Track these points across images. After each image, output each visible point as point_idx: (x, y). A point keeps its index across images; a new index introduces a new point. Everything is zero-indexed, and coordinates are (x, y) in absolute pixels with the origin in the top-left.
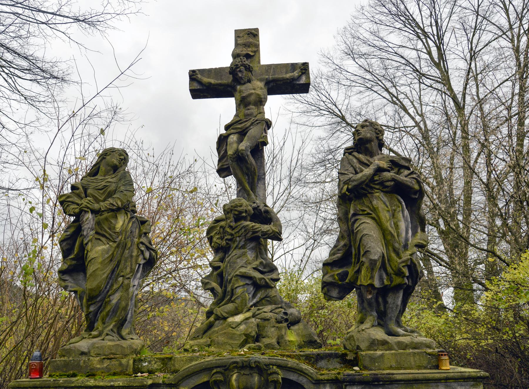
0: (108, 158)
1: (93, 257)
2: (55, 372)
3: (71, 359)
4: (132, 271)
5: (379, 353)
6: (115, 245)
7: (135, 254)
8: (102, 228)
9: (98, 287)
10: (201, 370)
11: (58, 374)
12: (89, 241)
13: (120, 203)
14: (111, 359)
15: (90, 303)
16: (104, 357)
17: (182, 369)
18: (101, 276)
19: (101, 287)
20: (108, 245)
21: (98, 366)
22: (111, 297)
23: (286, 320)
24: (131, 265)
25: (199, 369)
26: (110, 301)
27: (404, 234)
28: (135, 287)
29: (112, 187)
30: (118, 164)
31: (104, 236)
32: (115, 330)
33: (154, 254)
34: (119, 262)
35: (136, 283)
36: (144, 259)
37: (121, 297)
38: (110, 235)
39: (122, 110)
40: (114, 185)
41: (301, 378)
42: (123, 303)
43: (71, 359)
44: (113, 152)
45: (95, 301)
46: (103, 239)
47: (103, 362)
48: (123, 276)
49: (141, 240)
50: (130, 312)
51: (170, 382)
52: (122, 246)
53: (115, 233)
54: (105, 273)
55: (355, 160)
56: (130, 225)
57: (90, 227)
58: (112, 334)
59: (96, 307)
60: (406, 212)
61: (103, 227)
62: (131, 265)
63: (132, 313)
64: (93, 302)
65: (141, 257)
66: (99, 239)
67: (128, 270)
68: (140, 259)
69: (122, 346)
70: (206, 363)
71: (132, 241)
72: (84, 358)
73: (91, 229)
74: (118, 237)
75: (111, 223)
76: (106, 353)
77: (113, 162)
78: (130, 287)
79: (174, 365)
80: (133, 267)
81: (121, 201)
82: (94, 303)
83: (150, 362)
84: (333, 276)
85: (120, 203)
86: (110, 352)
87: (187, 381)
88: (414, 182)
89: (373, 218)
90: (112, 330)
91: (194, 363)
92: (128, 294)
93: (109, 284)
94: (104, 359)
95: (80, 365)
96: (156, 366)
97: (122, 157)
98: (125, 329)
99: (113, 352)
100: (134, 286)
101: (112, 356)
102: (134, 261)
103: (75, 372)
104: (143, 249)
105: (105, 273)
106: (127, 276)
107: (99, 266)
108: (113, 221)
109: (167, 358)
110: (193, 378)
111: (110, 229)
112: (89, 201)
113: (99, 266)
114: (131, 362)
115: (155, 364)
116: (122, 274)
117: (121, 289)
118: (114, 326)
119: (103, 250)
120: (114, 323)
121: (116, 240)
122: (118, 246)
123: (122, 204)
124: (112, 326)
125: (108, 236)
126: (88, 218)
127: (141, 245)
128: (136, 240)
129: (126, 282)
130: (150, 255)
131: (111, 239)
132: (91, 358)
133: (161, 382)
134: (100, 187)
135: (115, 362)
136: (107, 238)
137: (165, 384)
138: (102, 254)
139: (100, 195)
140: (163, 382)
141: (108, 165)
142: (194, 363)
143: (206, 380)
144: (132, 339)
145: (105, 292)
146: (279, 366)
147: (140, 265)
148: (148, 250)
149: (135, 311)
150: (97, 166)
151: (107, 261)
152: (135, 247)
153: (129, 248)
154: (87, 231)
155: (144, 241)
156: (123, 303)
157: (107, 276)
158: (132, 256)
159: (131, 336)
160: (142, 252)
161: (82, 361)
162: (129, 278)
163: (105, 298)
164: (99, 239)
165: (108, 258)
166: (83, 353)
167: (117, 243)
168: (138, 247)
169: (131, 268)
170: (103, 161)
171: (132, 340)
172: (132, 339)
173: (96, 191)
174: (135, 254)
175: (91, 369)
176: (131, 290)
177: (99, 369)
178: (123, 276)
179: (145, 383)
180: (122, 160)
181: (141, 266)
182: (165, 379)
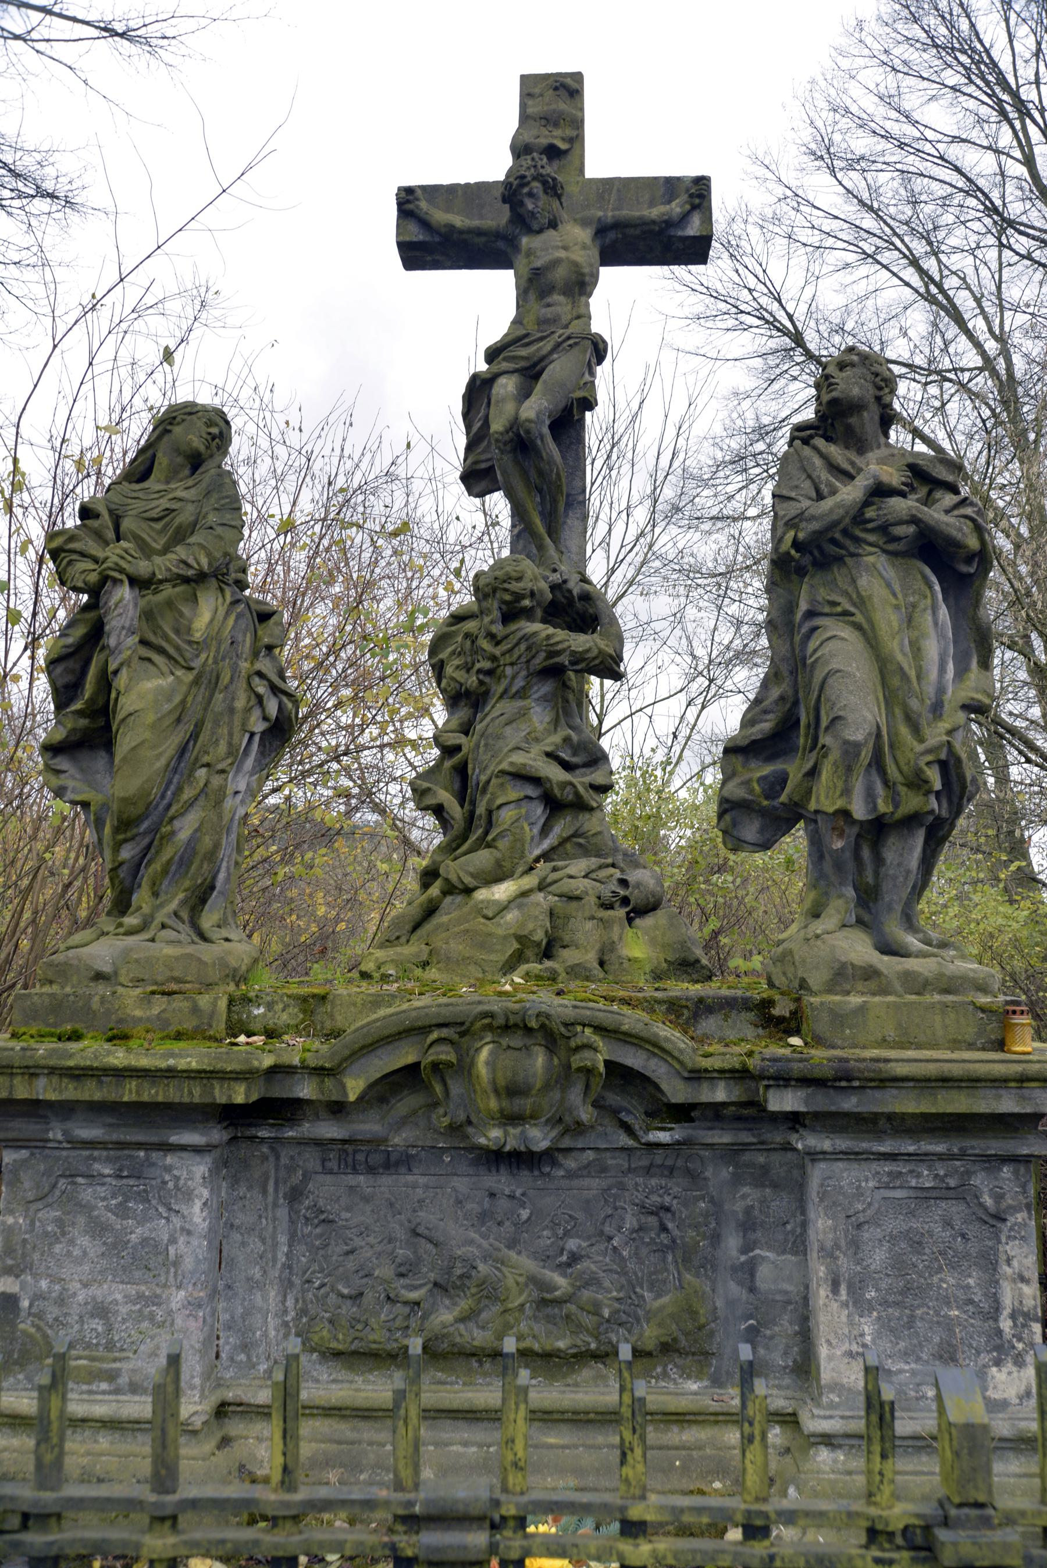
0: (177, 430)
1: (131, 709)
2: (26, 1024)
3: (68, 990)
4: (232, 751)
6: (190, 677)
7: (240, 704)
8: (156, 629)
11: (33, 1031)
12: (122, 664)
13: (204, 562)
15: (121, 837)
21: (138, 1013)
22: (177, 824)
23: (625, 901)
24: (231, 734)
25: (394, 1030)
26: (173, 833)
27: (933, 675)
31: (161, 651)
33: (290, 705)
34: (199, 726)
35: (242, 786)
36: (265, 718)
38: (178, 648)
41: (653, 1063)
45: (135, 831)
48: (207, 765)
49: (258, 666)
52: (208, 682)
54: (160, 754)
55: (818, 462)
56: (231, 621)
59: (138, 850)
60: (943, 612)
62: (231, 734)
64: (129, 834)
65: (257, 713)
67: (222, 748)
68: (253, 719)
69: (199, 960)
70: (414, 1014)
71: (235, 668)
72: (102, 989)
79: (332, 1016)
80: (236, 740)
81: (209, 555)
82: (132, 839)
83: (270, 1006)
86: (168, 974)
88: (967, 527)
89: (858, 627)
91: (382, 1012)
92: (220, 817)
93: (172, 787)
94: (153, 993)
96: (285, 1016)
99: (176, 974)
101: (174, 987)
103: (78, 1026)
104: (261, 690)
105: (160, 754)
106: (220, 767)
107: (147, 735)
108: (186, 610)
109: (314, 996)
110: (379, 1052)
111: (177, 632)
113: (147, 735)
114: (223, 1004)
116: (206, 759)
117: (201, 801)
118: (183, 903)
120: (181, 896)
122: (196, 682)
124: (176, 902)
125: (171, 651)
127: (256, 680)
128: (244, 665)
129: (216, 781)
130: (281, 708)
132: (120, 990)
133: (296, 1061)
134: (154, 514)
135: (179, 1003)
136: (170, 657)
140: (302, 1061)
141: (178, 451)
142: (382, 1012)
143: (411, 1059)
144: (227, 940)
147: (252, 734)
150: (149, 453)
151: (167, 722)
155: (264, 670)
156: (207, 842)
158: (232, 710)
159: (224, 933)
160: (260, 698)
161: (97, 999)
162: (223, 771)
164: (149, 660)
165: (170, 712)
166: (99, 976)
169: (230, 744)
170: (166, 439)
172: (227, 940)
173: (144, 525)
174: (240, 704)
175: (120, 1021)
176: (229, 803)
177: (140, 1019)
178: (207, 765)
179: (256, 1063)
181: (257, 738)
182: (307, 1055)
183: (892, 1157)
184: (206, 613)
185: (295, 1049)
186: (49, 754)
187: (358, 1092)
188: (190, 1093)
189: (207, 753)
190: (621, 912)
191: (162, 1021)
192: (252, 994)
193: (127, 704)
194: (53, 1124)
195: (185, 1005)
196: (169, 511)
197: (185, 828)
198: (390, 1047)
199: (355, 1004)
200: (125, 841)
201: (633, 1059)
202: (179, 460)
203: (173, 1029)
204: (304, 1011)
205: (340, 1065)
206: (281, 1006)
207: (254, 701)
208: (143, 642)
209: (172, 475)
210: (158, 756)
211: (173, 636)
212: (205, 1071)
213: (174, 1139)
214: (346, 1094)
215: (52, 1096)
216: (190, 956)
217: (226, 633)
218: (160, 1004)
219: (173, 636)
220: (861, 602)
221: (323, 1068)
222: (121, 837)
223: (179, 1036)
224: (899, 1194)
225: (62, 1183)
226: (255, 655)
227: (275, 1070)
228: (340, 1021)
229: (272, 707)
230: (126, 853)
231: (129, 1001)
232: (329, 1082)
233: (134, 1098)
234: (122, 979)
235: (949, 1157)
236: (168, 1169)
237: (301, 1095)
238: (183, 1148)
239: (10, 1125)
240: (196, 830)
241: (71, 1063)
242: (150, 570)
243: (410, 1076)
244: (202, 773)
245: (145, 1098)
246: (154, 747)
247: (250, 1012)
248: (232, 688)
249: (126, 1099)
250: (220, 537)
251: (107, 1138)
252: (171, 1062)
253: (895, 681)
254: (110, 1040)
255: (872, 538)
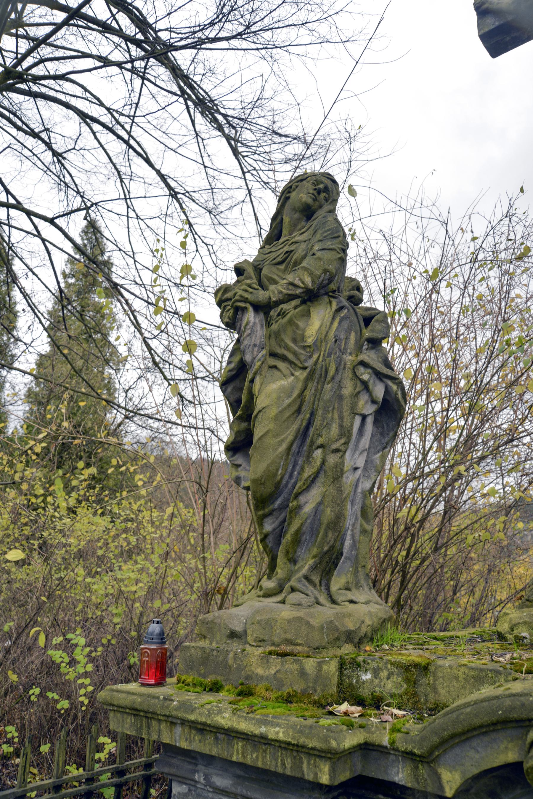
0: (293, 195)
1: (264, 405)
2: (187, 673)
3: (214, 645)
4: (345, 433)
6: (305, 374)
7: (348, 390)
8: (281, 343)
9: (270, 474)
10: (494, 724)
11: (189, 680)
12: (255, 374)
13: (308, 280)
14: (284, 655)
15: (260, 513)
16: (273, 648)
17: (456, 704)
18: (275, 450)
19: (275, 475)
20: (293, 378)
21: (260, 671)
22: (302, 499)
24: (341, 418)
25: (486, 720)
26: (299, 507)
28: (359, 472)
29: (300, 251)
30: (310, 201)
31: (284, 359)
32: (316, 579)
33: (395, 387)
34: (313, 414)
35: (361, 462)
36: (374, 402)
37: (323, 497)
38: (295, 354)
39: (363, 132)
40: (303, 246)
42: (328, 511)
43: (214, 645)
44: (302, 180)
45: (271, 507)
46: (281, 365)
47: (268, 662)
48: (322, 446)
49: (361, 357)
50: (349, 532)
51: (410, 748)
52: (316, 376)
53: (304, 348)
54: (283, 441)
56: (336, 324)
57: (258, 343)
58: (304, 589)
59: (277, 523)
61: (282, 340)
62: (341, 418)
63: (353, 536)
64: (267, 510)
65: (364, 398)
66: (275, 367)
67: (335, 430)
68: (361, 403)
69: (308, 623)
70: (508, 702)
71: (339, 363)
72: (235, 646)
73: (259, 346)
74: (310, 357)
75: (297, 327)
76: (276, 640)
77: (300, 201)
78: (342, 473)
79: (435, 689)
80: (346, 422)
81: (311, 274)
82: (270, 514)
83: (376, 672)
85: (308, 280)
86: (283, 636)
87: (457, 750)
90: (306, 578)
91: (487, 691)
92: (340, 491)
93: (298, 468)
94: (270, 653)
95: (227, 663)
96: (390, 685)
97: (321, 186)
98: (339, 575)
99: (289, 636)
100: (356, 469)
101: (288, 649)
102: (346, 408)
103: (220, 678)
104: (365, 377)
105: (283, 441)
106: (334, 447)
107: (271, 426)
108: (301, 324)
109: (416, 665)
110: (475, 743)
111: (295, 341)
112: (250, 286)
113: (271, 426)
114: (332, 667)
115: (388, 678)
116: (320, 441)
117: (322, 478)
118: (314, 568)
119: (282, 389)
120: (311, 562)
121: (306, 364)
122: (310, 378)
123: (313, 282)
124: (307, 567)
125: (290, 356)
126: (247, 324)
127: (361, 369)
128: (349, 359)
129: (332, 459)
130: (387, 390)
131: (297, 362)
132: (248, 648)
133: (385, 741)
134: (279, 259)
135: (290, 665)
136: (291, 363)
137: (397, 750)
138: (279, 398)
139: (280, 274)
140: (393, 743)
141: (294, 210)
142: (487, 691)
143: (511, 757)
144: (352, 602)
145: (290, 486)
147: (364, 417)
148: (381, 380)
149: (364, 532)
150: (279, 218)
151: (287, 414)
152: (348, 374)
153: (333, 378)
154: (252, 352)
155: (366, 359)
156: (328, 513)
157: (289, 448)
158: (340, 398)
159: (350, 595)
160: (365, 385)
161: (231, 655)
162: (337, 451)
163: (288, 500)
164: (275, 367)
165: (289, 405)
166: (233, 635)
167: (308, 370)
168: (354, 373)
169: (341, 426)
170: (287, 204)
171: (352, 606)
172: (352, 602)
173: (274, 269)
174: (348, 390)
175: (248, 677)
176: (349, 479)
177: (262, 677)
178: (322, 446)
179: (334, 744)
180: (319, 193)
181: (370, 420)
182: (398, 735)
184: (318, 321)
185: (393, 725)
186: (230, 453)
187: (455, 786)
188: (283, 764)
189: (320, 435)
191: (277, 681)
192: (360, 659)
193: (260, 403)
194: (200, 767)
195: (295, 667)
196: (289, 253)
197: (310, 502)
198: (486, 739)
199: (457, 678)
200: (265, 516)
202: (297, 215)
203: (286, 690)
204: (407, 681)
205: (431, 752)
206: (385, 674)
207: (359, 387)
208: (273, 355)
209: (294, 226)
210: (280, 443)
211: (292, 345)
212: (289, 744)
214: (441, 787)
215: (184, 745)
216: (300, 619)
217: (332, 335)
218: (276, 663)
219: (292, 345)
221: (412, 753)
222: (260, 513)
223: (288, 700)
226: (359, 349)
227: (367, 748)
228: (443, 694)
229: (379, 391)
230: (269, 526)
231: (254, 660)
232: (423, 770)
233: (241, 760)
234: (250, 639)
237: (396, 779)
239: (174, 761)
240: (320, 504)
241: (192, 717)
242: (267, 296)
244: (318, 454)
245: (249, 761)
246: (277, 435)
247: (358, 677)
248: (338, 378)
249: (234, 759)
250: (320, 259)
251: (233, 790)
252: (263, 729)
254: (239, 694)
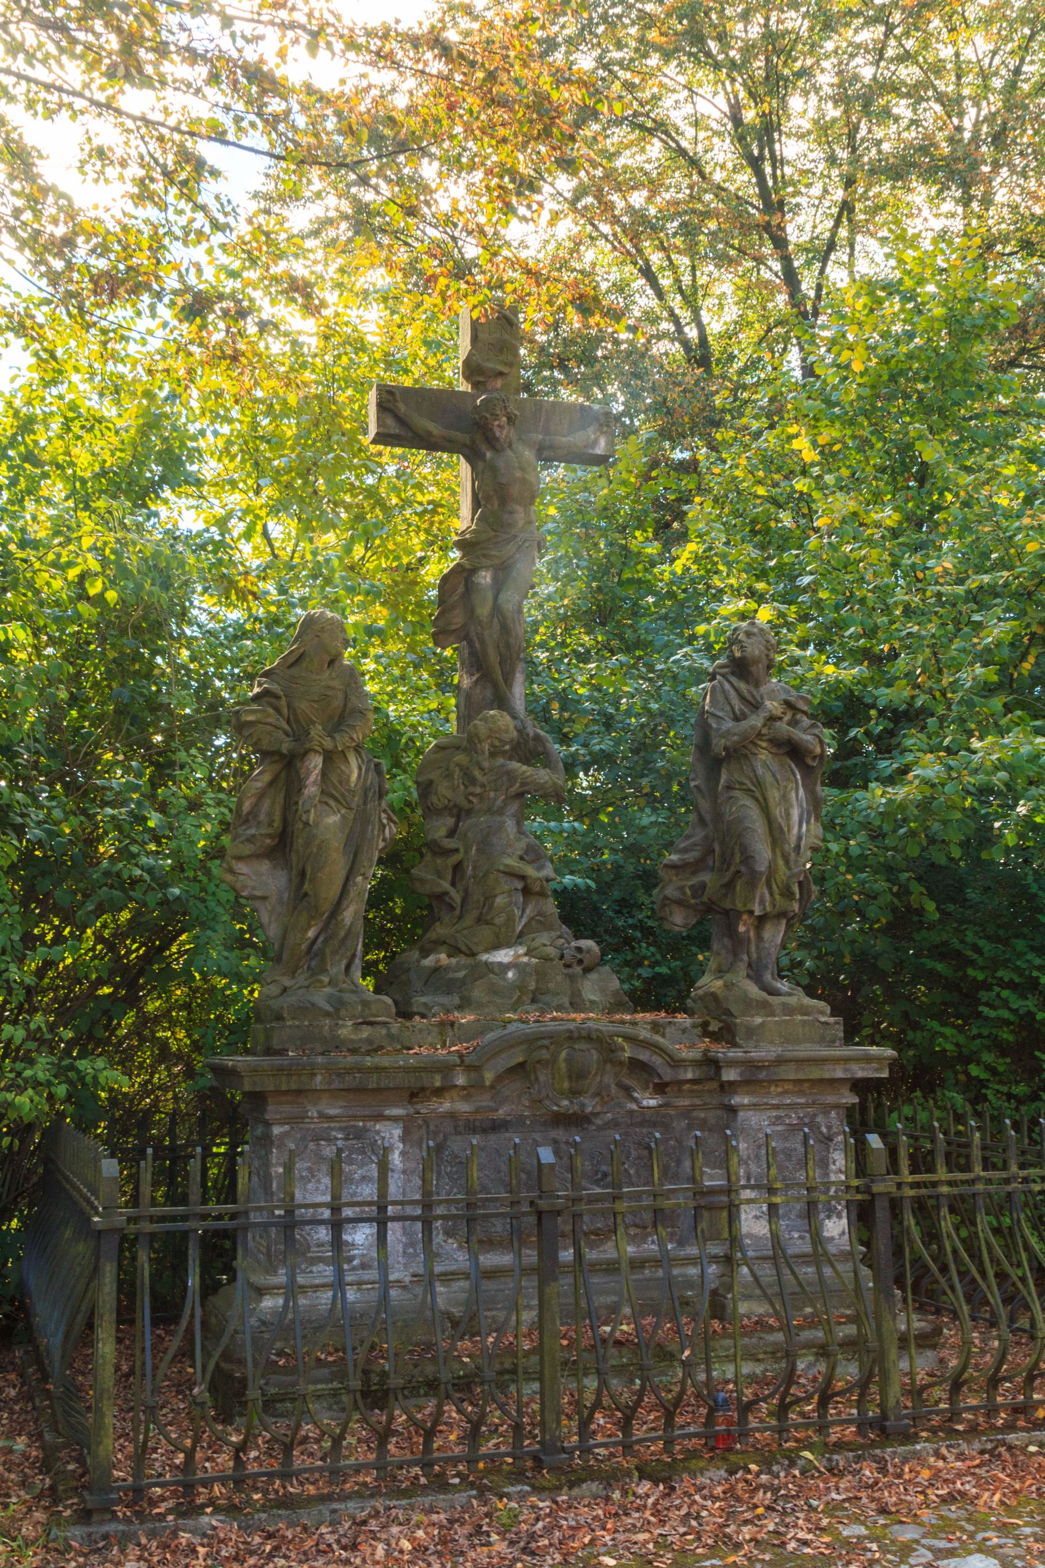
5: (759, 1020)
23: (580, 962)
27: (795, 831)
41: (654, 1058)
46: (332, 803)
55: (733, 694)
60: (801, 791)
84: (681, 889)
88: (816, 742)
89: (757, 800)
142: (490, 1036)
146: (627, 1038)
183: (777, 1107)
190: (578, 969)
201: (644, 1056)
213: (387, 1112)
220: (759, 784)
224: (780, 1128)
225: (312, 1146)
235: (807, 1105)
236: (378, 1132)
238: (389, 1118)
243: (519, 1069)
253: (777, 834)
255: (764, 744)
